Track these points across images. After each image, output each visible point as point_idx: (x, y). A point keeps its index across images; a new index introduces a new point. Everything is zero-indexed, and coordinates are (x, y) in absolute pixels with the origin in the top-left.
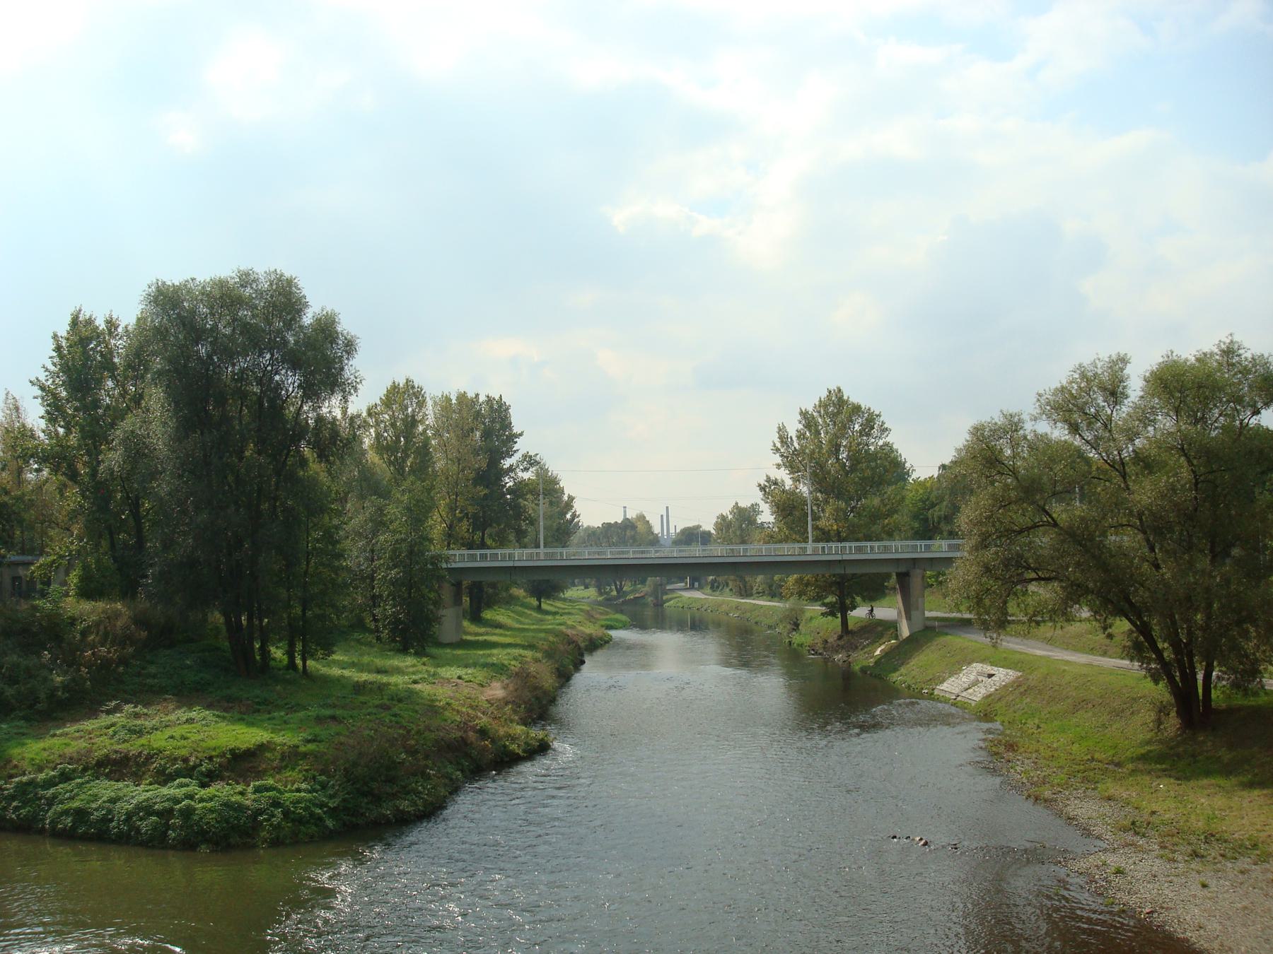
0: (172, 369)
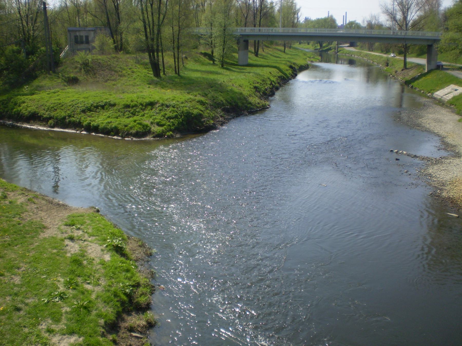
0: (426, 11)
